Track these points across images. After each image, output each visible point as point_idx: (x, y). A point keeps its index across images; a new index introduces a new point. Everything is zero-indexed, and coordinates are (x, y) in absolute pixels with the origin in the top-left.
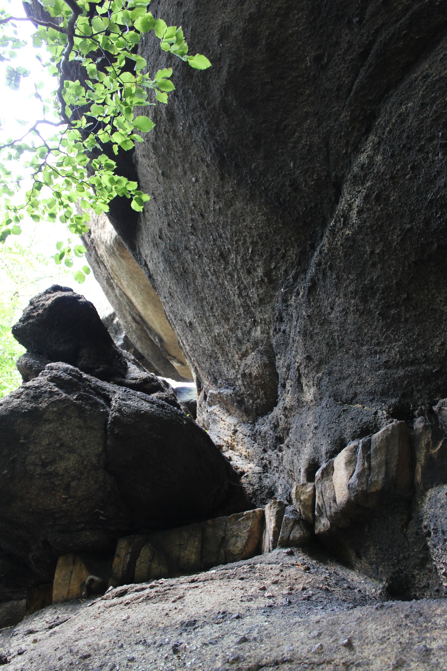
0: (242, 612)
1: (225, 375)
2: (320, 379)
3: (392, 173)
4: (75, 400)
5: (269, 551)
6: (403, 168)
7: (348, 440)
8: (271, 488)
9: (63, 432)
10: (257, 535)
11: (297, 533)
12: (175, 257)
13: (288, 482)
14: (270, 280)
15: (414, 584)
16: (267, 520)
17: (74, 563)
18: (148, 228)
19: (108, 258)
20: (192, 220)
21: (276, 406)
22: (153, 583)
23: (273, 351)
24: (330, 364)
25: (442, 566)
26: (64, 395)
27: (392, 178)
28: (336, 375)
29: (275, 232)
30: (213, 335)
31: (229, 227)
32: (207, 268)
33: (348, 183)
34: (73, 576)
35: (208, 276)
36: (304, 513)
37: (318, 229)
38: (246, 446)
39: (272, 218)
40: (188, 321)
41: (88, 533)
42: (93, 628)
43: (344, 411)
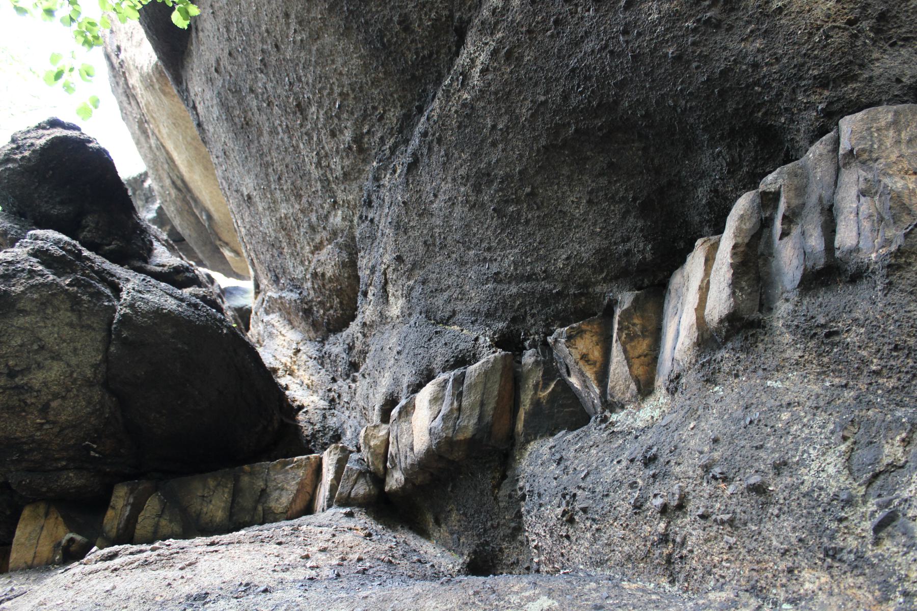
0: (272, 584)
1: (289, 273)
2: (412, 289)
3: (530, 25)
4: (68, 285)
5: (323, 510)
6: (544, 21)
7: (437, 371)
8: (337, 430)
9: (44, 330)
10: (309, 489)
11: (361, 489)
12: (235, 102)
13: (359, 423)
14: (359, 147)
15: (501, 560)
16: (324, 470)
17: (47, 515)
18: (201, 55)
19: (143, 92)
20: (263, 51)
21: (353, 320)
22: (157, 545)
23: (355, 246)
24: (426, 269)
25: (534, 537)
26: (51, 277)
27: (529, 32)
28: (432, 285)
29: (372, 83)
30: (278, 216)
31: (311, 68)
32: (278, 122)
33: (474, 30)
34: (44, 533)
35: (278, 134)
36: (373, 463)
37: (430, 87)
38: (310, 372)
39: (370, 64)
40: (246, 193)
41: (71, 475)
42: (61, 601)
43: (436, 333)
